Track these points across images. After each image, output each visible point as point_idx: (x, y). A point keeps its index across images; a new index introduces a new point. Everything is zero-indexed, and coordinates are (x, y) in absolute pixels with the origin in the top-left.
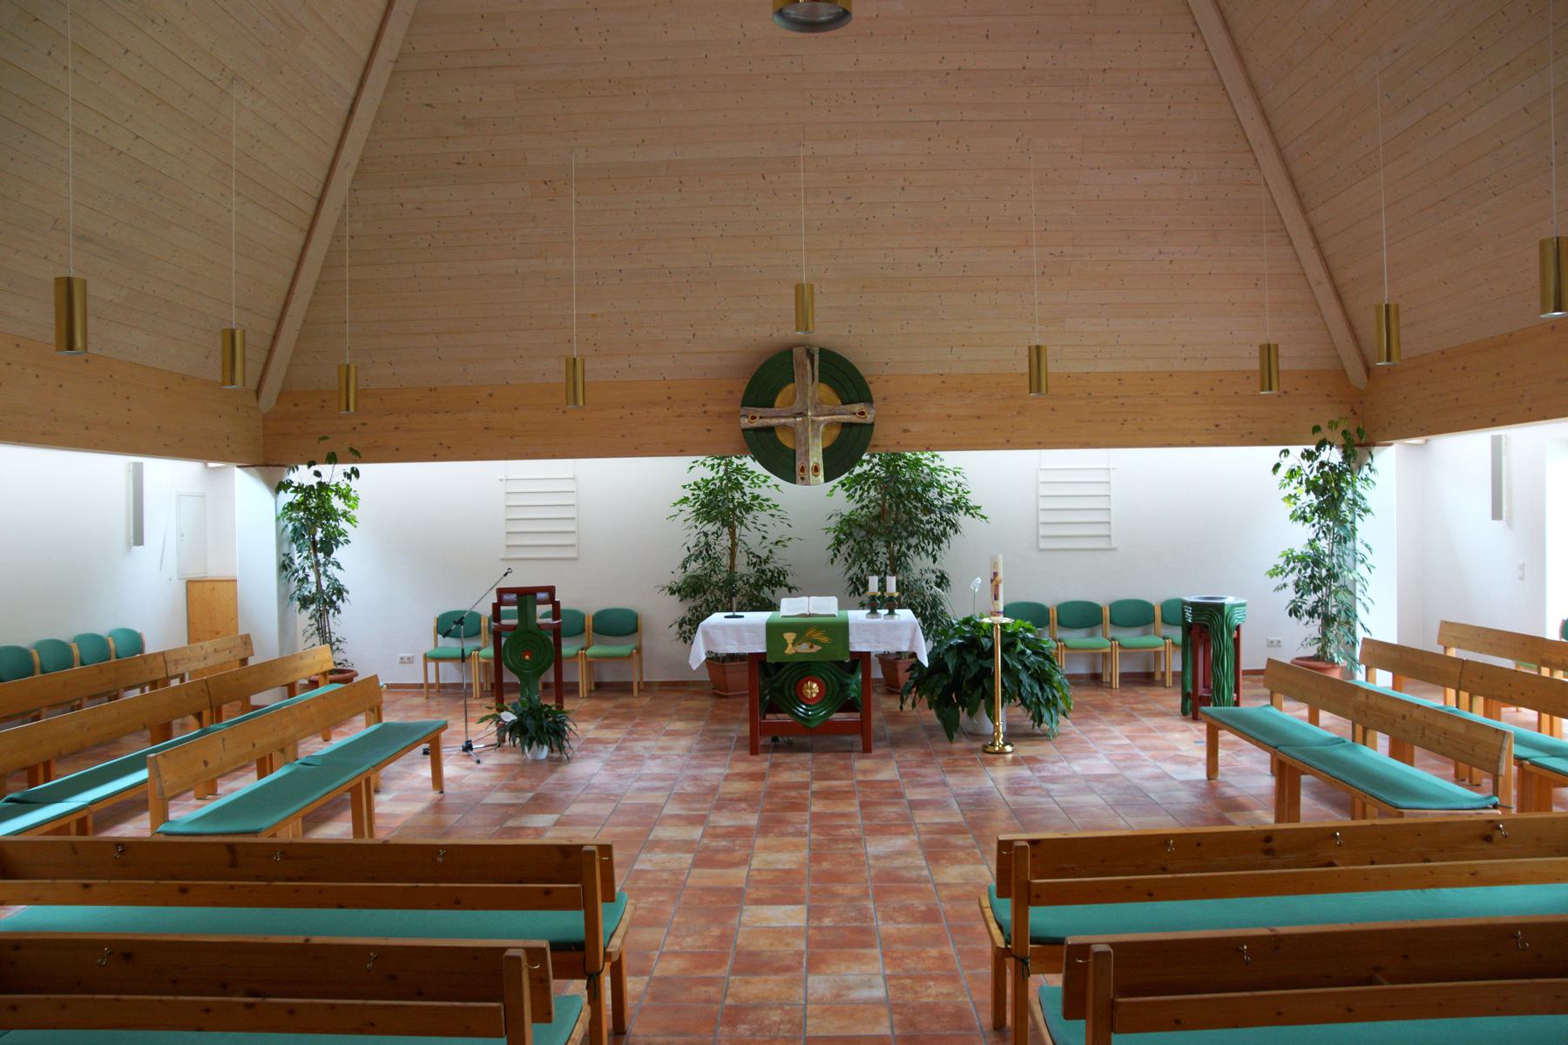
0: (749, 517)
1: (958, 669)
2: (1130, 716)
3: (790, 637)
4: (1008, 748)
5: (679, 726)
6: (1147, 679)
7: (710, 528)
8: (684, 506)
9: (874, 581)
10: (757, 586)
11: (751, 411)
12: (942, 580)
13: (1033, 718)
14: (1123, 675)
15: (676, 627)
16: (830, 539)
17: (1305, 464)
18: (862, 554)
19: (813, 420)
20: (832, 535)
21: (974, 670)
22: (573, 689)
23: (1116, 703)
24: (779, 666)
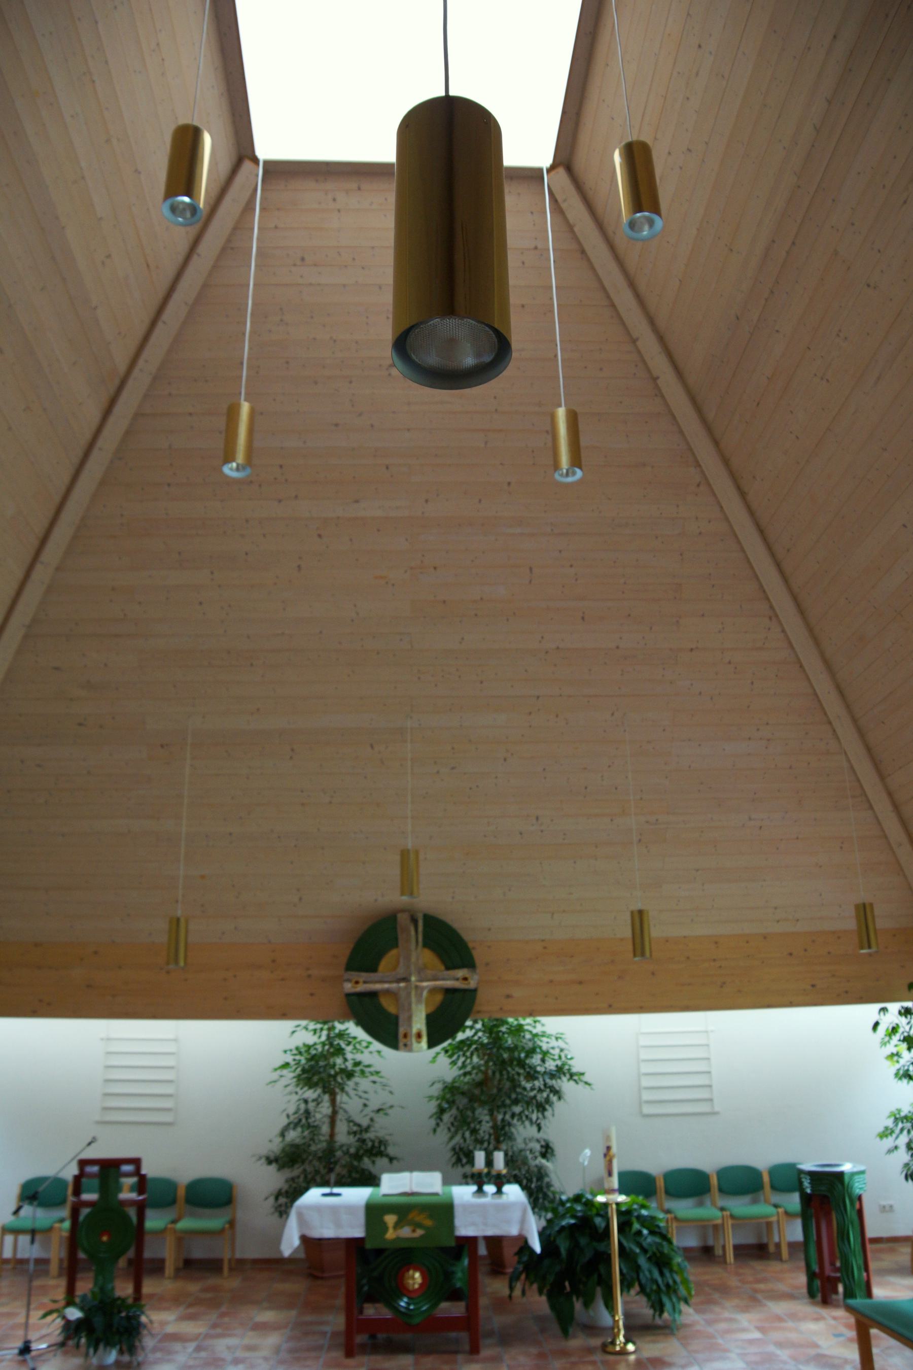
0: (351, 1083)
1: (570, 1253)
2: (753, 1301)
3: (390, 1219)
4: (631, 1347)
5: (267, 1316)
6: (758, 1251)
7: (310, 1094)
8: (285, 1072)
9: (480, 1157)
10: (357, 1157)
11: (354, 975)
12: (547, 1151)
13: (653, 1306)
14: (737, 1248)
15: (272, 1200)
16: (432, 1107)
17: (903, 1021)
18: (464, 1122)
19: (416, 988)
21: (588, 1255)
22: (158, 1267)
23: (734, 1282)
24: (379, 1252)
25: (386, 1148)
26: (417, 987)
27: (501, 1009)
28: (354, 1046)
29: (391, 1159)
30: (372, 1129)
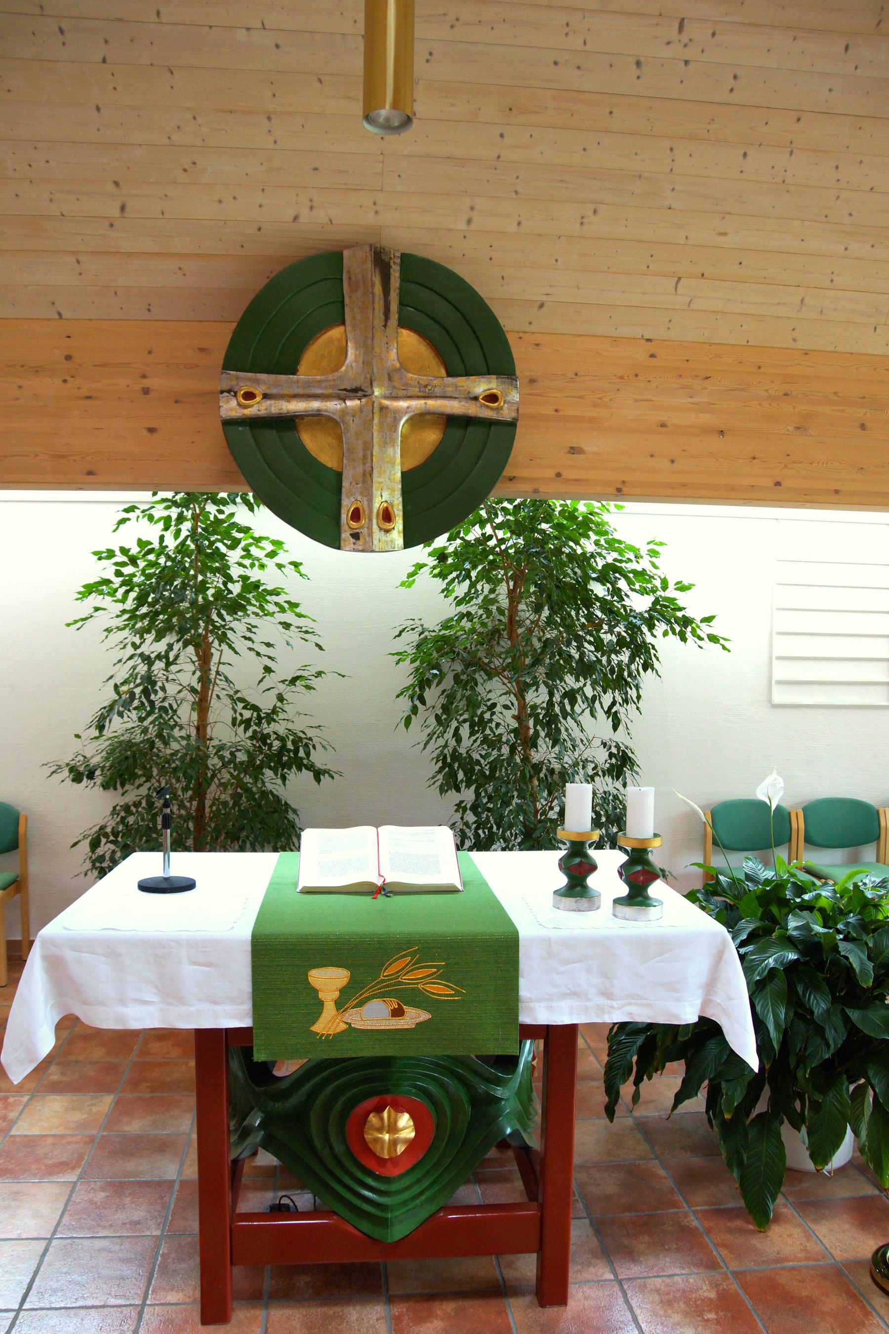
0: (238, 626)
7: (152, 646)
10: (253, 768)
11: (245, 381)
15: (85, 846)
16: (404, 675)
19: (383, 400)
20: (407, 667)
25: (308, 754)
26: (383, 408)
27: (559, 475)
28: (246, 549)
29: (318, 775)
30: (281, 716)
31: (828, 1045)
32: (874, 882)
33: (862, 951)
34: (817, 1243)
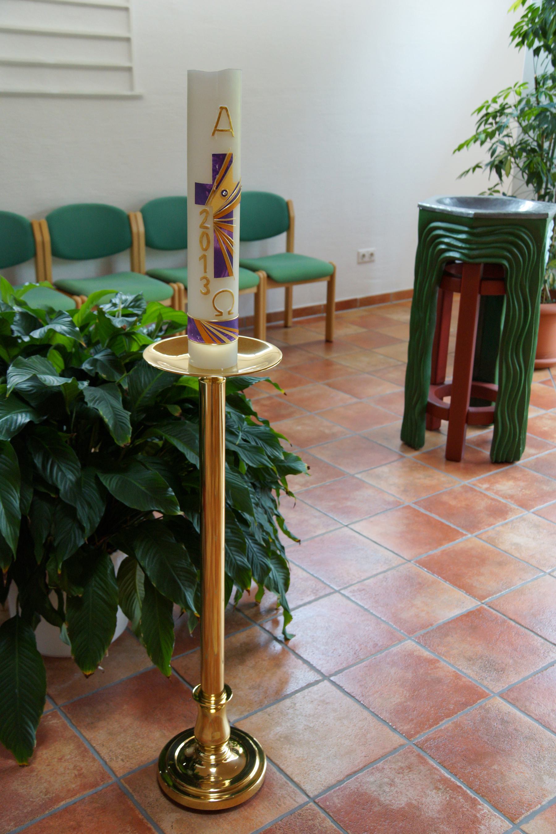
31: (82, 528)
32: (126, 300)
33: (116, 397)
34: (94, 760)
